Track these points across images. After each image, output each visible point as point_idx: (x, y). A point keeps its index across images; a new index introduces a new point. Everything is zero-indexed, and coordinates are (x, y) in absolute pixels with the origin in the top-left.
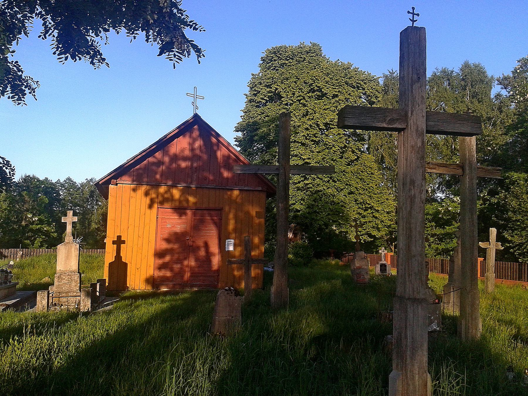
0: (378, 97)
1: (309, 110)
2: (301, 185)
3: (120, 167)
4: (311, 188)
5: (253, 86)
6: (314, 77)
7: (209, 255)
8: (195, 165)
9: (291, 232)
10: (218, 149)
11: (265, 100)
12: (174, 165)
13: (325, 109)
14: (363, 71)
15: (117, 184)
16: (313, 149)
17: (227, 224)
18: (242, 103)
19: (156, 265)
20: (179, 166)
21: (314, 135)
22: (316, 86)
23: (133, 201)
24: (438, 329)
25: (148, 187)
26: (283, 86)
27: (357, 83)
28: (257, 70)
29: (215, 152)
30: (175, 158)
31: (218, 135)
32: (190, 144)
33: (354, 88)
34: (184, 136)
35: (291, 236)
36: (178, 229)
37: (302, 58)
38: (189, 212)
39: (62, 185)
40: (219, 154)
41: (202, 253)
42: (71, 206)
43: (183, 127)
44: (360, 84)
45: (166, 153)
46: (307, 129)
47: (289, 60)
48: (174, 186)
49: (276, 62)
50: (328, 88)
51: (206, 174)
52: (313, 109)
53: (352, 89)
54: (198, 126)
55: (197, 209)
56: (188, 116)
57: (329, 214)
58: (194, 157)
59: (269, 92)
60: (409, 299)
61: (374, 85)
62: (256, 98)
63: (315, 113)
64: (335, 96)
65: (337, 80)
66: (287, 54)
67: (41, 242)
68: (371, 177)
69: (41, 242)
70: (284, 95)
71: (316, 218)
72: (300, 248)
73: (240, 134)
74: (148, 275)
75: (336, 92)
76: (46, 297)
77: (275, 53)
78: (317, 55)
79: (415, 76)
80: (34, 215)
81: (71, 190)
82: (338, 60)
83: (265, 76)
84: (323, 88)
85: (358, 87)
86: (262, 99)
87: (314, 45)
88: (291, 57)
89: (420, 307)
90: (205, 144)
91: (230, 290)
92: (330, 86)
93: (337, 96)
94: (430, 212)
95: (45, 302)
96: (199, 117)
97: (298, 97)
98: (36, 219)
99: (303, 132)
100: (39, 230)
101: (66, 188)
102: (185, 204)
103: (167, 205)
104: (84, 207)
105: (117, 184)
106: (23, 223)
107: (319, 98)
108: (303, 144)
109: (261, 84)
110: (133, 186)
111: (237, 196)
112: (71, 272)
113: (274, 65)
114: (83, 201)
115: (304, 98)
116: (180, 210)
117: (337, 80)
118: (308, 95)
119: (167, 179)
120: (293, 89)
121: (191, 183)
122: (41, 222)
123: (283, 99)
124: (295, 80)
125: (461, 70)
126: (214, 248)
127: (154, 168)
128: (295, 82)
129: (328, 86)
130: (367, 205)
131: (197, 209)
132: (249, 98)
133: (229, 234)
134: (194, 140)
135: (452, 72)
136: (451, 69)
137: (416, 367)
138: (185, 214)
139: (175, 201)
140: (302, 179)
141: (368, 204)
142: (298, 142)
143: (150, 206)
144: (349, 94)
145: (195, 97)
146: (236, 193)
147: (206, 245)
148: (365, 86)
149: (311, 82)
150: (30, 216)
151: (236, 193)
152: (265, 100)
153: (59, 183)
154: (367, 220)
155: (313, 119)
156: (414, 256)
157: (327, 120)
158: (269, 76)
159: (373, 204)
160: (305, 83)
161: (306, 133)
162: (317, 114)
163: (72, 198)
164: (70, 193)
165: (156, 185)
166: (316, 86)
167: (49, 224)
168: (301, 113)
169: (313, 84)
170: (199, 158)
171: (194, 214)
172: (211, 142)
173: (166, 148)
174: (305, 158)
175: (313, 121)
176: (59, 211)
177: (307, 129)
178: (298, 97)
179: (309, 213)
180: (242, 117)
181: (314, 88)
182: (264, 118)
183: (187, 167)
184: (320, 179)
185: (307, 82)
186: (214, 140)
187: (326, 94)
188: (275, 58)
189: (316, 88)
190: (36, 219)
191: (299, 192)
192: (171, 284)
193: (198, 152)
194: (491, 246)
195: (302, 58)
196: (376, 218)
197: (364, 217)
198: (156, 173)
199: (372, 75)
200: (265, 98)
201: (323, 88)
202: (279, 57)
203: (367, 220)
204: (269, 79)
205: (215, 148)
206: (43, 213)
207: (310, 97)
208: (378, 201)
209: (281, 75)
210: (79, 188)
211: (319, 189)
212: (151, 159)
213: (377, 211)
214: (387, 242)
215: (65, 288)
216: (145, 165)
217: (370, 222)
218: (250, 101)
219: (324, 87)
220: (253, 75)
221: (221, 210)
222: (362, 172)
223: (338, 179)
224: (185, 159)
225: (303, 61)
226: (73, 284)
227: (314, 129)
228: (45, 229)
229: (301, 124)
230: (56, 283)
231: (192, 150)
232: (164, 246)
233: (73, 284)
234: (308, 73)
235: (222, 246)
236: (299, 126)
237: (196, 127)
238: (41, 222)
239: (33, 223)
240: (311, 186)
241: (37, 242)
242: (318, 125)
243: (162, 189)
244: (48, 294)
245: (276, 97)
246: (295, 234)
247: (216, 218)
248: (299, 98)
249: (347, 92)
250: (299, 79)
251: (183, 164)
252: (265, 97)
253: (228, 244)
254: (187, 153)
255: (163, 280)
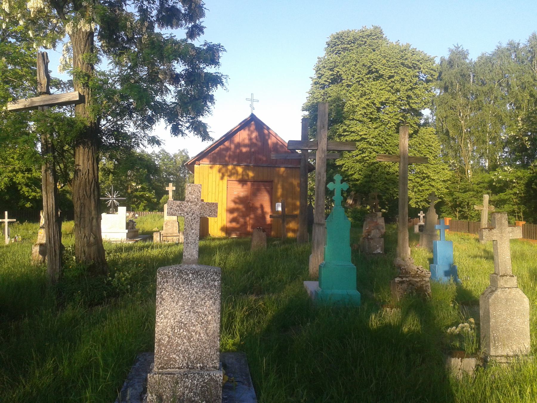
0: (434, 75)
1: (367, 91)
2: (358, 158)
3: (202, 153)
4: (368, 160)
5: (318, 70)
6: (372, 60)
7: (264, 213)
8: (253, 150)
9: (351, 199)
10: (269, 138)
11: (328, 82)
12: (238, 151)
13: (381, 90)
14: (421, 51)
15: (199, 165)
16: (370, 126)
17: (276, 192)
18: (308, 85)
19: (228, 220)
20: (241, 151)
21: (371, 113)
22: (374, 68)
23: (210, 176)
24: (381, 252)
25: (221, 166)
26: (344, 69)
27: (413, 63)
28: (322, 54)
29: (267, 140)
30: (238, 145)
31: (268, 129)
32: (249, 135)
33: (410, 68)
34: (244, 130)
35: (351, 202)
36: (242, 194)
37: (363, 41)
38: (249, 184)
39: (158, 156)
40: (270, 142)
41: (259, 211)
42: (166, 175)
43: (243, 123)
44: (415, 64)
45: (232, 142)
46: (364, 108)
47: (350, 44)
48: (238, 165)
49: (339, 46)
50: (384, 70)
51: (260, 156)
52: (370, 90)
53: (408, 70)
54: (255, 122)
55: (254, 181)
56: (246, 116)
57: (385, 183)
58: (251, 145)
59: (331, 75)
60: (317, 224)
61: (429, 65)
62: (320, 80)
63: (372, 93)
64: (390, 77)
65: (393, 62)
66: (349, 39)
67: (144, 206)
68: (428, 148)
69: (144, 206)
70: (345, 77)
71: (373, 186)
72: (359, 212)
73: (307, 113)
74: (222, 225)
75: (392, 73)
76: (159, 236)
77: (338, 38)
78: (378, 37)
79: (322, 126)
80: (137, 184)
81: (165, 160)
82: (398, 41)
83: (328, 60)
84: (380, 70)
85: (414, 67)
86: (326, 81)
87: (376, 28)
88: (353, 41)
89: (321, 228)
90: (259, 135)
91: (260, 228)
92: (386, 68)
93: (392, 77)
94: (486, 181)
95: (158, 239)
96: (255, 116)
97: (357, 78)
98: (140, 186)
99: (360, 111)
100: (142, 196)
101: (161, 159)
102: (246, 178)
103: (233, 178)
104: (177, 176)
105: (199, 165)
106: (129, 191)
107: (376, 79)
108: (360, 121)
109: (325, 68)
110: (210, 165)
111: (284, 172)
112: (173, 221)
113: (337, 49)
114: (176, 170)
115: (363, 80)
116: (242, 181)
117: (393, 62)
118: (366, 76)
119: (233, 160)
120: (353, 72)
121: (250, 163)
122: (143, 189)
123: (343, 81)
124: (355, 63)
125: (528, 41)
126: (268, 209)
127: (224, 152)
128: (355, 65)
129: (385, 68)
130: (424, 175)
131: (254, 181)
132: (314, 81)
133: (278, 198)
134: (252, 132)
135: (519, 44)
136: (517, 41)
137: (319, 252)
138: (246, 184)
139: (239, 175)
140: (360, 152)
141: (425, 173)
142: (356, 120)
143: (222, 178)
144: (405, 75)
145: (252, 100)
146: (282, 169)
147: (262, 207)
148: (421, 66)
149: (369, 64)
150: (134, 184)
151: (282, 169)
152: (328, 82)
153: (154, 154)
154: (423, 188)
155: (369, 99)
156: (319, 206)
157: (383, 99)
158: (331, 60)
159: (429, 174)
160: (363, 65)
161: (363, 112)
162: (373, 94)
163: (166, 167)
164: (164, 163)
165: (226, 165)
166: (374, 68)
167: (150, 191)
168: (359, 93)
169: (371, 66)
170: (255, 145)
171: (253, 185)
172: (264, 133)
173: (232, 139)
174: (362, 134)
175: (369, 101)
176: (156, 179)
177: (364, 108)
178: (357, 78)
179: (366, 182)
180: (308, 98)
181: (372, 70)
182: (327, 98)
183: (246, 152)
184: (376, 152)
185: (366, 64)
186: (266, 132)
187: (383, 75)
188: (338, 43)
189: (374, 70)
190: (140, 186)
191: (357, 164)
192: (238, 233)
193: (254, 141)
194: (485, 208)
195: (363, 41)
196: (433, 186)
197: (421, 185)
198: (225, 156)
199: (428, 55)
200: (328, 80)
201: (380, 70)
202: (342, 42)
203: (423, 188)
204: (332, 63)
205: (267, 137)
206: (144, 182)
207: (368, 78)
208: (435, 171)
209: (343, 59)
210: (172, 158)
211: (375, 161)
212: (222, 147)
213: (433, 180)
214: (452, 208)
215: (170, 231)
216: (218, 151)
217: (427, 190)
218: (316, 83)
219: (380, 69)
220: (319, 58)
221: (271, 182)
222: (420, 144)
223: (393, 152)
224: (245, 146)
225: (364, 44)
226: (175, 228)
227: (371, 108)
228: (147, 195)
229: (358, 103)
230: (164, 228)
231: (250, 139)
232: (232, 205)
233: (175, 228)
234: (367, 56)
235: (273, 207)
236: (357, 106)
237: (253, 123)
238: (143, 189)
239: (137, 190)
240: (368, 158)
241: (141, 207)
242: (374, 104)
243: (230, 167)
244: (160, 235)
245: (336, 80)
246: (355, 201)
247: (268, 188)
248: (358, 80)
249: (402, 73)
250: (358, 62)
251: (244, 150)
252: (328, 79)
253: (277, 206)
254: (247, 141)
255: (232, 230)
